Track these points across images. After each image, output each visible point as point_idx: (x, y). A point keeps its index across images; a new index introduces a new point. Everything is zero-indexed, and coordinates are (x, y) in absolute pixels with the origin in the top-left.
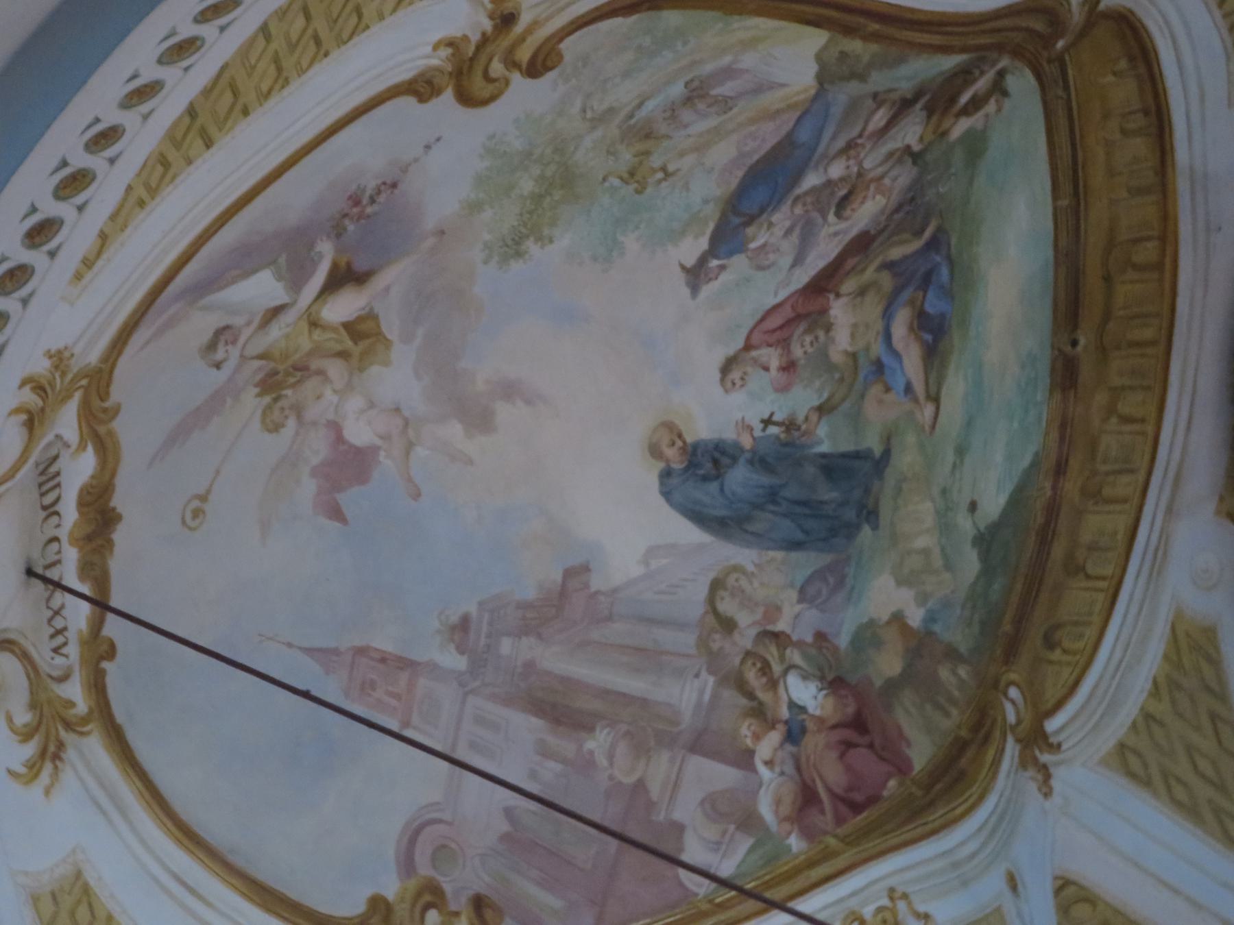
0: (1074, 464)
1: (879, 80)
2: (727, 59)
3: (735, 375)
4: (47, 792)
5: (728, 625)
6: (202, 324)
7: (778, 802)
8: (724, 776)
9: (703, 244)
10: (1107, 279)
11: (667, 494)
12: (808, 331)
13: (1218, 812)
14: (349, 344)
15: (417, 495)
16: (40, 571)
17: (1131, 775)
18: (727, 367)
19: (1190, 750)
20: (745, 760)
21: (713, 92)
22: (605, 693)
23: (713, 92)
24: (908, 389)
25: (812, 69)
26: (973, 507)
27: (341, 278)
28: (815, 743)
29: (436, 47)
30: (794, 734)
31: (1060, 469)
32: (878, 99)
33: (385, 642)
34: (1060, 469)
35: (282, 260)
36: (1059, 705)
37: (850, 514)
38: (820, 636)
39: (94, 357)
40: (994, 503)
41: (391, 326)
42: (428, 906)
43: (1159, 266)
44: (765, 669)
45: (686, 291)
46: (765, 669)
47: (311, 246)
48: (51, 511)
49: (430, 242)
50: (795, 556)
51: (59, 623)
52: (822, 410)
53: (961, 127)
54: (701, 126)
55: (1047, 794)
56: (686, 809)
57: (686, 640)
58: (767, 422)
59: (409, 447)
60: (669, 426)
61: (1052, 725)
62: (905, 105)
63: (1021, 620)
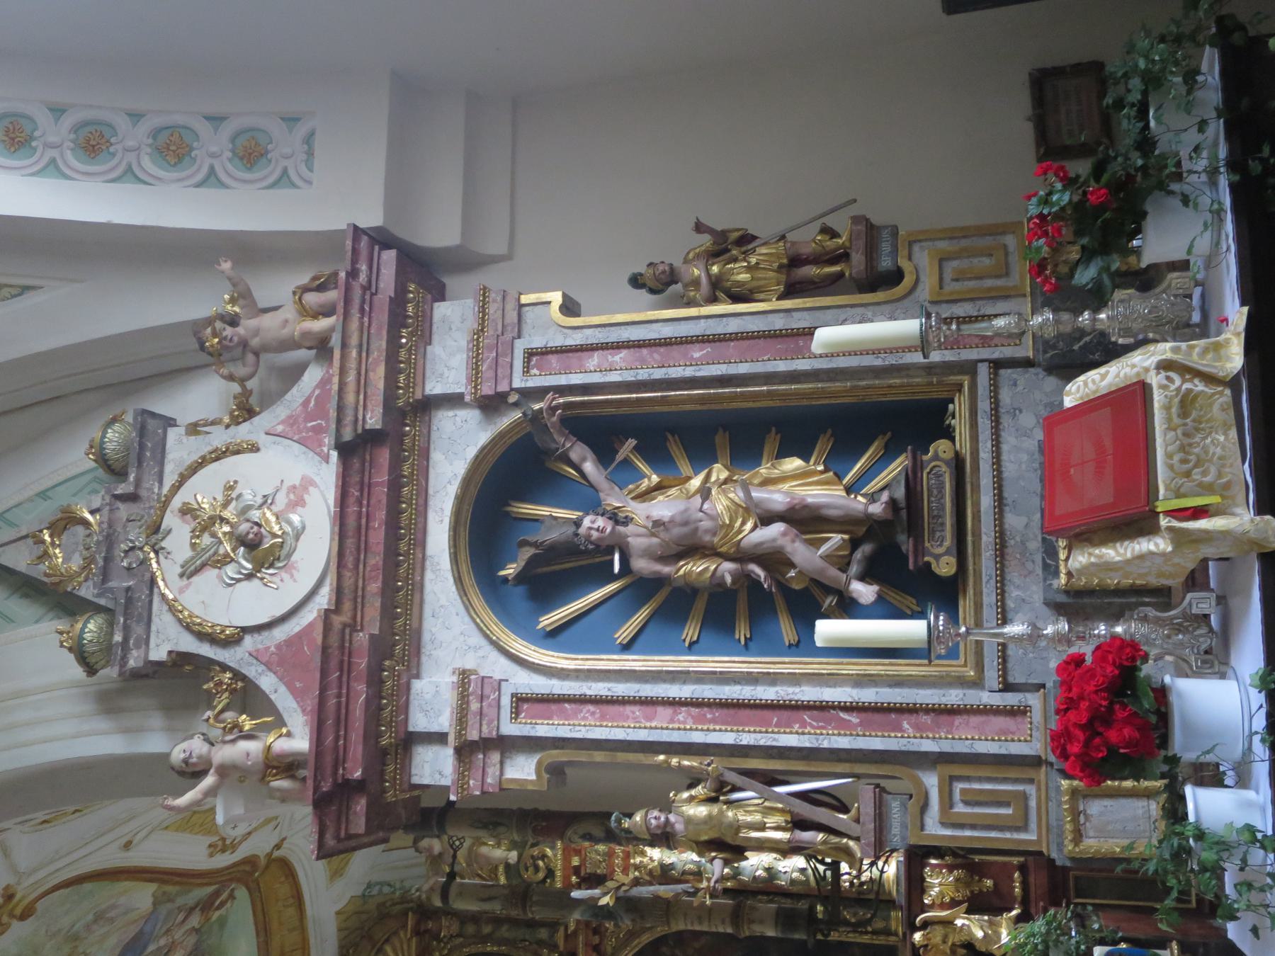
1: (180, 901)
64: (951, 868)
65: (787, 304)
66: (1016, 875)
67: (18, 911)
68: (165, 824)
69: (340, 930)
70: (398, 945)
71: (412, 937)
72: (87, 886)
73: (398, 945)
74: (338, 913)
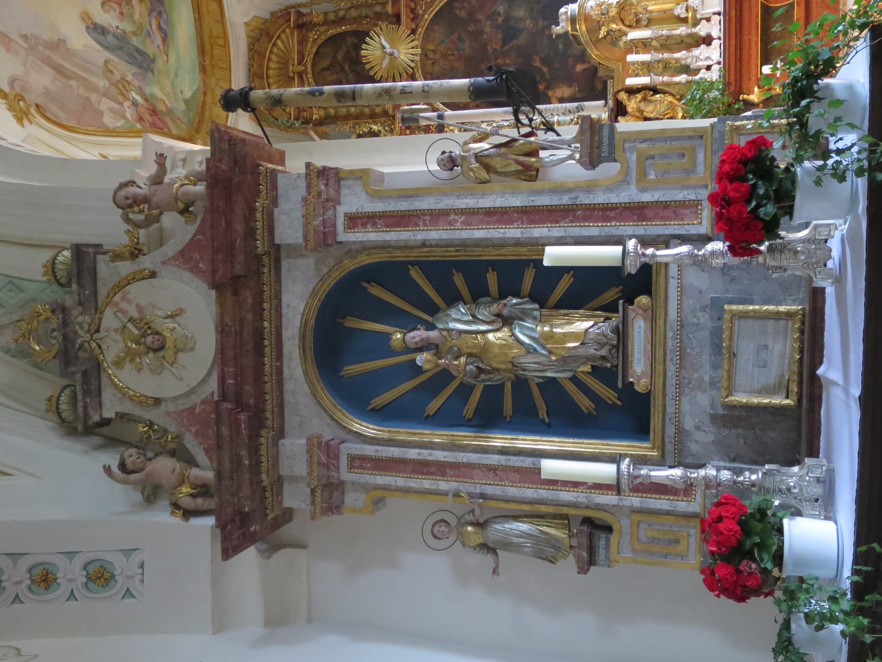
0: (209, 94)
3: (106, 8)
7: (132, 117)
8: (116, 106)
11: (89, 34)
20: (121, 104)
24: (158, 46)
26: (181, 92)
30: (135, 104)
31: (205, 94)
34: (205, 94)
40: (188, 94)
42: (19, 100)
43: (224, 46)
58: (117, 27)
65: (652, 433)
69: (248, 36)
74: (246, 24)
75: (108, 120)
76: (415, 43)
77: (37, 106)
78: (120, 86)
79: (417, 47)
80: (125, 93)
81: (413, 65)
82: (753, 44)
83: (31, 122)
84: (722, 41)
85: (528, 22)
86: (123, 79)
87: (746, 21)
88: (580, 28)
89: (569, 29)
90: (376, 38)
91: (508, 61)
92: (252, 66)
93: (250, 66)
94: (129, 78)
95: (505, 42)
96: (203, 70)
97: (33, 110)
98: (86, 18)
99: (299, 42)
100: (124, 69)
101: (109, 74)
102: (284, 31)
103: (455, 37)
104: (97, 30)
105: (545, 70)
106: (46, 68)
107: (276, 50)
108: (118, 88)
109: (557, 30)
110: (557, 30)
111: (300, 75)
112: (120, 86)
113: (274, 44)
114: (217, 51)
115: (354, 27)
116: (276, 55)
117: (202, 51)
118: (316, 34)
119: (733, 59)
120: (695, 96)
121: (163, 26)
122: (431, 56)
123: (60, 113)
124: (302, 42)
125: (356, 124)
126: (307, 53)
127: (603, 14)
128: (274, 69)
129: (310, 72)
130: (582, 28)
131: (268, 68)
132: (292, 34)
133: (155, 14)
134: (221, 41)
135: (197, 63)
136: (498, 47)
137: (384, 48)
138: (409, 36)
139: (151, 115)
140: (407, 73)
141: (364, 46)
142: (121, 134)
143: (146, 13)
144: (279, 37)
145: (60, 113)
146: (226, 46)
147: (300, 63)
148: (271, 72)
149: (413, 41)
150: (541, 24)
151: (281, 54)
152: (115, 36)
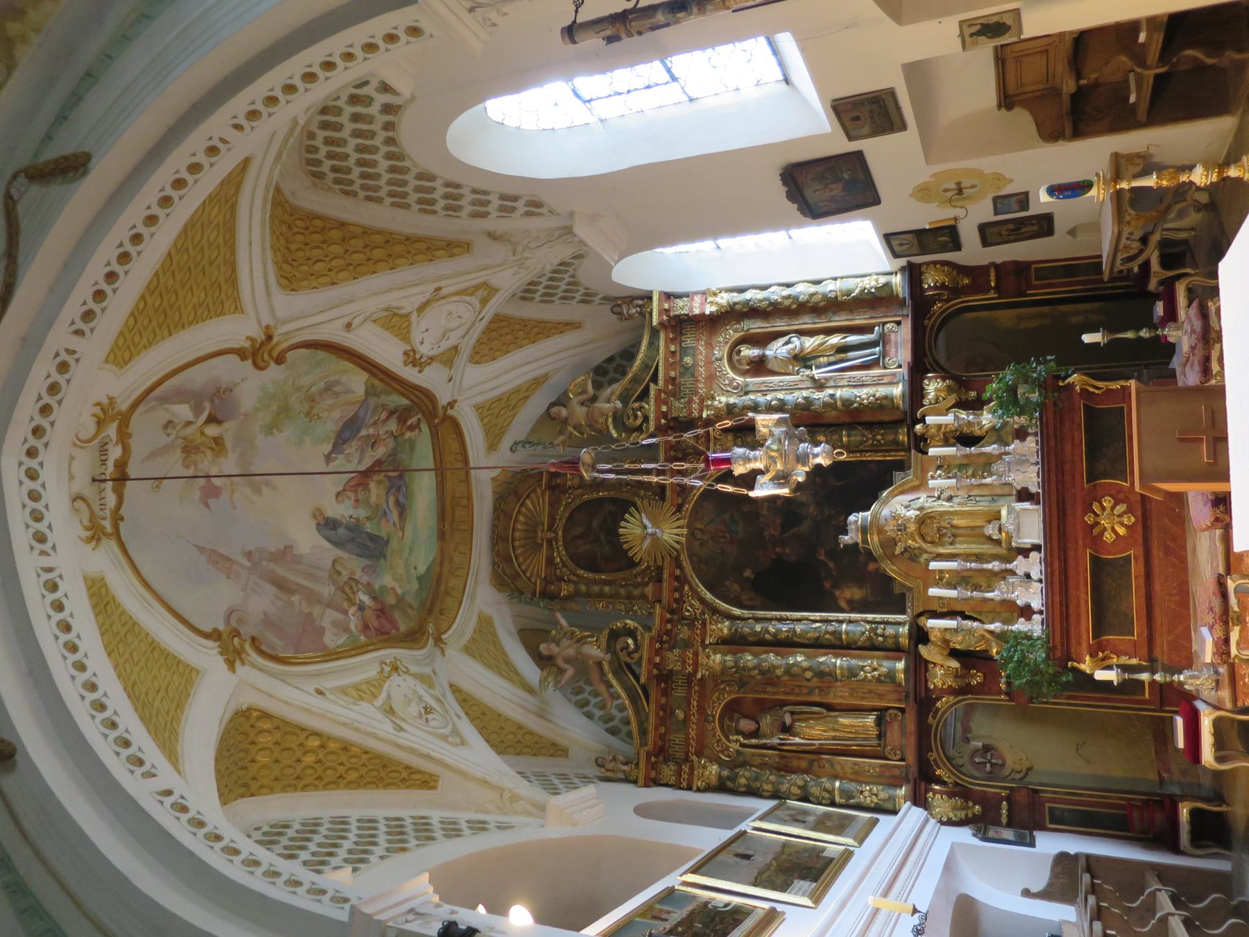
0: (446, 564)
1: (384, 399)
2: (337, 377)
3: (340, 498)
4: (94, 549)
5: (339, 573)
6: (162, 415)
7: (356, 627)
8: (339, 616)
9: (330, 447)
10: (453, 508)
11: (319, 530)
12: (363, 490)
13: (497, 667)
14: (214, 445)
15: (235, 508)
16: (97, 478)
17: (469, 654)
18: (338, 494)
19: (487, 650)
20: (345, 612)
21: (335, 389)
22: (298, 584)
23: (335, 389)
24: (394, 524)
25: (363, 388)
26: (415, 568)
27: (212, 419)
28: (368, 613)
29: (248, 338)
30: (362, 608)
31: (441, 564)
32: (384, 406)
33: (222, 550)
34: (441, 564)
35: (193, 403)
36: (445, 632)
37: (378, 553)
38: (369, 584)
39: (124, 406)
40: (422, 569)
41: (228, 443)
42: (234, 636)
43: (468, 507)
44: (351, 588)
45: (325, 464)
46: (351, 588)
47: (202, 403)
48: (104, 462)
49: (242, 417)
50: (360, 559)
51: (103, 501)
52: (368, 518)
53: (408, 435)
54: (329, 402)
55: (444, 655)
56: (325, 623)
57: (326, 575)
58: (351, 517)
59: (232, 492)
60: (319, 510)
61: (444, 637)
62: (391, 413)
63: (432, 603)
64: (944, 379)
66: (1004, 803)
67: (275, 354)
68: (374, 317)
69: (494, 492)
70: (535, 500)
71: (546, 489)
72: (321, 354)
73: (535, 500)
74: (494, 479)
75: (332, 639)
76: (681, 522)
77: (253, 639)
78: (347, 589)
79: (682, 535)
80: (351, 596)
81: (678, 547)
82: (1083, 602)
83: (243, 663)
84: (1043, 585)
85: (811, 509)
86: (351, 579)
87: (1071, 573)
88: (872, 539)
89: (859, 541)
90: (637, 516)
91: (787, 551)
92: (497, 527)
93: (494, 528)
94: (358, 575)
95: (785, 527)
96: (442, 536)
97: (247, 646)
98: (318, 514)
99: (550, 505)
100: (354, 564)
101: (335, 577)
102: (534, 490)
103: (727, 516)
104: (328, 526)
105: (831, 565)
106: (268, 586)
107: (524, 510)
108: (343, 591)
109: (846, 539)
110: (846, 539)
111: (549, 542)
112: (347, 589)
113: (522, 504)
114: (459, 513)
115: (613, 494)
116: (525, 515)
117: (442, 515)
118: (569, 497)
119: (1057, 618)
120: (1013, 657)
121: (401, 499)
122: (699, 535)
123: (276, 641)
124: (554, 504)
125: (611, 603)
126: (558, 517)
127: (899, 530)
128: (521, 530)
129: (561, 539)
130: (874, 540)
131: (514, 530)
132: (543, 494)
133: (393, 491)
134: (464, 502)
135: (435, 529)
136: (776, 533)
137: (645, 527)
138: (673, 514)
139: (378, 617)
140: (670, 556)
141: (623, 524)
142: (342, 655)
143: (383, 492)
144: (528, 497)
145: (276, 641)
146: (469, 507)
147: (550, 529)
148: (517, 534)
149: (678, 520)
150: (827, 512)
151: (529, 515)
152: (348, 528)
